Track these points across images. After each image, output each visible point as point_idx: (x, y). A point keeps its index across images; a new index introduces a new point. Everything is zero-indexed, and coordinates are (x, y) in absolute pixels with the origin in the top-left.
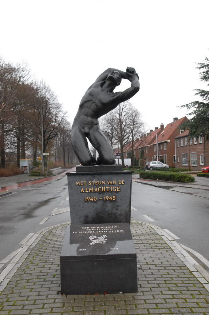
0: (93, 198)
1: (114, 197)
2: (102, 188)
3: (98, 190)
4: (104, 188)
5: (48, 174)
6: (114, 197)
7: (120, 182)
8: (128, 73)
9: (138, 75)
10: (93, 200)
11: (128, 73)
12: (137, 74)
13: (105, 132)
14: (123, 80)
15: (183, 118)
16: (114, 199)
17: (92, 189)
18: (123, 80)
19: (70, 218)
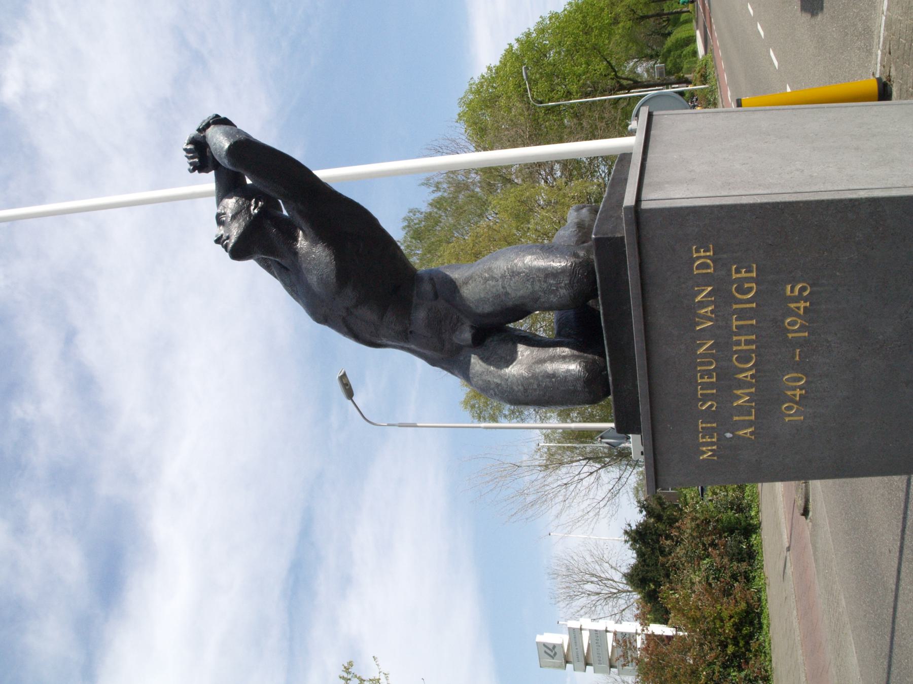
0: (794, 388)
1: (792, 291)
2: (736, 352)
3: (750, 369)
4: (738, 343)
5: (648, 532)
6: (792, 291)
7: (704, 266)
8: (192, 161)
9: (222, 115)
10: (801, 388)
11: (192, 161)
12: (199, 130)
13: (679, 639)
14: (212, 174)
15: (251, 139)
16: (803, 289)
17: (739, 392)
18: (212, 174)
19: (886, 479)
